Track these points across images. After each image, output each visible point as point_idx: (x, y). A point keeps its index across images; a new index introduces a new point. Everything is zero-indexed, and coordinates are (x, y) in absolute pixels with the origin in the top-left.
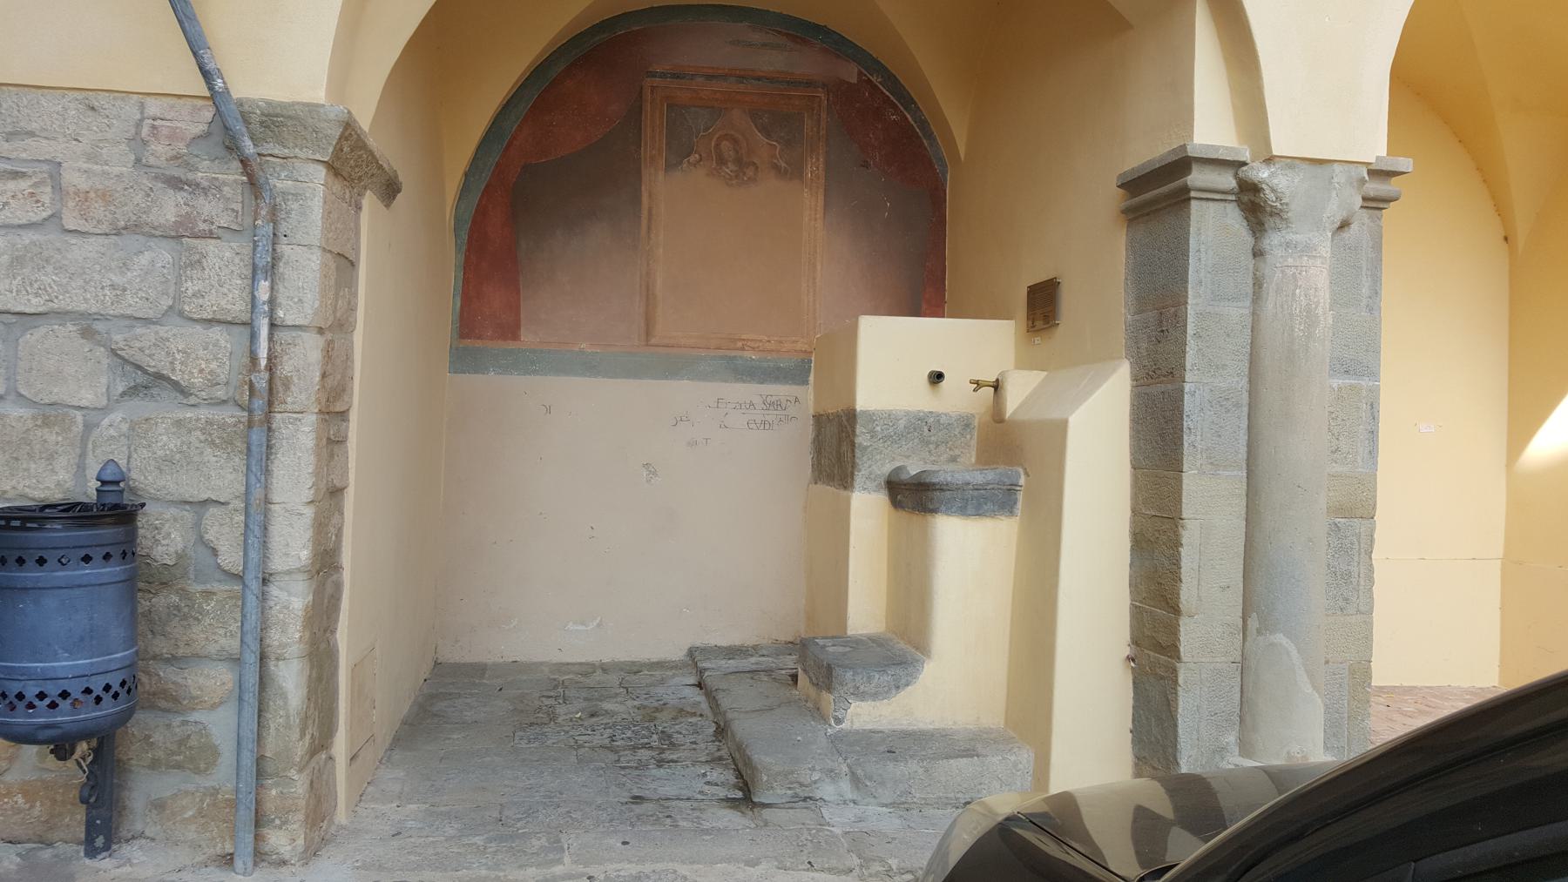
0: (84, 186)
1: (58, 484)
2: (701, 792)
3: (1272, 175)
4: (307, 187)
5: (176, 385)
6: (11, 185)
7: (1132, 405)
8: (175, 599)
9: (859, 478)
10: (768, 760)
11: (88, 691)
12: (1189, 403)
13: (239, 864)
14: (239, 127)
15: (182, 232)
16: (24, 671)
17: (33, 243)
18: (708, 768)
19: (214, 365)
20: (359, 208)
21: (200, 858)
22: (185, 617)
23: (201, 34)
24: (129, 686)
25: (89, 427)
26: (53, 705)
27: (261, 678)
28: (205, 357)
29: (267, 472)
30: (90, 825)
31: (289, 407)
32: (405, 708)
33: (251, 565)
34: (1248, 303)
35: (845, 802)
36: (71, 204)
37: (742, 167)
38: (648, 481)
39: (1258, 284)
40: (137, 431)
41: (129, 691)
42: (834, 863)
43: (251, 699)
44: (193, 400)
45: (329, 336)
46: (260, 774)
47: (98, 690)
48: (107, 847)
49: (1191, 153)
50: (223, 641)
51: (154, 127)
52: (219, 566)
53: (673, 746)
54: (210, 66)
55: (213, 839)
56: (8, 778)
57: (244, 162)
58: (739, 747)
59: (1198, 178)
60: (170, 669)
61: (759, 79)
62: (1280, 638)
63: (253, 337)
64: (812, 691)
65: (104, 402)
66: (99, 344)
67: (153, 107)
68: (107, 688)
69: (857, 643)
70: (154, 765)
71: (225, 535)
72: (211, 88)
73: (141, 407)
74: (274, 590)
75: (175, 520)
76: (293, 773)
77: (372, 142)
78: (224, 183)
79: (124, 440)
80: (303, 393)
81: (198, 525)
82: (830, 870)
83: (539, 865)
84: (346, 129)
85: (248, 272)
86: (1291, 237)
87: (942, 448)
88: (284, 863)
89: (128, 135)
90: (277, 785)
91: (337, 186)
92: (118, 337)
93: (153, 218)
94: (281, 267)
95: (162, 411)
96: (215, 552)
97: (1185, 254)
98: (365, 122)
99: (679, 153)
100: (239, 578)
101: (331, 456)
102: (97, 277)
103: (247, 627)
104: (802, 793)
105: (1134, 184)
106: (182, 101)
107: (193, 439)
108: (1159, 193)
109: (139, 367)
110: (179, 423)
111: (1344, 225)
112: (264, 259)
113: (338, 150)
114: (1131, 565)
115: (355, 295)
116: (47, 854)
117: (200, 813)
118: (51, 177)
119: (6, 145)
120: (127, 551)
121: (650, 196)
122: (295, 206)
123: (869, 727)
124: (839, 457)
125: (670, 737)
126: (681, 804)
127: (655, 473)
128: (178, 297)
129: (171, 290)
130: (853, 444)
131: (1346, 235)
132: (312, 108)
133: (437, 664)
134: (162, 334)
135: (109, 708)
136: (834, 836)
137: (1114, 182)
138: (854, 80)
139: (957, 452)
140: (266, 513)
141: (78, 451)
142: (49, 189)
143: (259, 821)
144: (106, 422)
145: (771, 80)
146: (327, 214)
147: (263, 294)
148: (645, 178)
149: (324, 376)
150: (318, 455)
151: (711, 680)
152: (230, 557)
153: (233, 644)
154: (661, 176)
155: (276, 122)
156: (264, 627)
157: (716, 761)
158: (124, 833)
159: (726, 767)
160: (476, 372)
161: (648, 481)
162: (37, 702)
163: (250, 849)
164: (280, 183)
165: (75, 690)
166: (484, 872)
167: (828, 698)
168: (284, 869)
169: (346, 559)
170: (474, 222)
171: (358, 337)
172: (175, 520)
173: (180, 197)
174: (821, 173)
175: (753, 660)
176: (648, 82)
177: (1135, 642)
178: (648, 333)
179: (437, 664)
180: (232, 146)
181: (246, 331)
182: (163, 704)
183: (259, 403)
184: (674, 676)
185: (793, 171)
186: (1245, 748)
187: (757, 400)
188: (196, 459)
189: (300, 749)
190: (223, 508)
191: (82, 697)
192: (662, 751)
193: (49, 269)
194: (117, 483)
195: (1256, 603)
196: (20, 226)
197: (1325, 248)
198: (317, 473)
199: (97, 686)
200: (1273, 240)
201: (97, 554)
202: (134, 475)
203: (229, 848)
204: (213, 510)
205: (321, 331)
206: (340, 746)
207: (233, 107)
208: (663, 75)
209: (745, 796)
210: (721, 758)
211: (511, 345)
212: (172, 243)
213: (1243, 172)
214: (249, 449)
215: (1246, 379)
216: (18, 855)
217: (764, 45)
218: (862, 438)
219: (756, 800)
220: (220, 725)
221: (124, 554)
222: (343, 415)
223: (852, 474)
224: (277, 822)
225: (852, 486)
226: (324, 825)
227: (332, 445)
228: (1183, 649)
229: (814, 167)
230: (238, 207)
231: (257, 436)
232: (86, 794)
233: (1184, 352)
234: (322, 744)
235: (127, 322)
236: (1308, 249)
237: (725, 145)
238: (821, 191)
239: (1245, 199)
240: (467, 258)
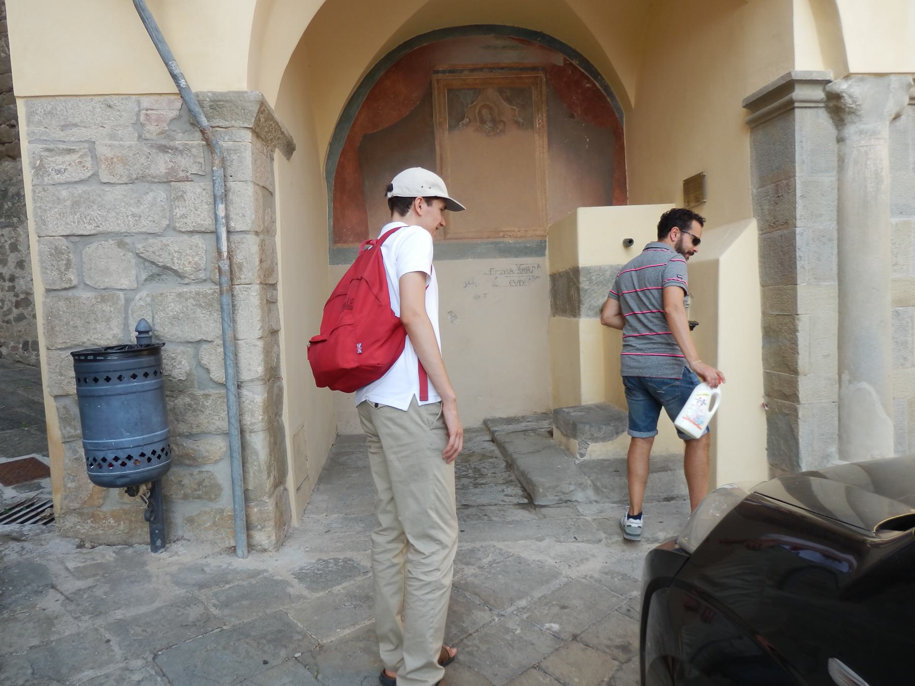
0: (110, 155)
1: (114, 336)
2: (502, 501)
3: (850, 86)
4: (241, 145)
5: (175, 272)
6: (68, 158)
7: (760, 247)
8: (188, 400)
9: (584, 309)
10: (542, 480)
11: (143, 455)
12: (799, 241)
13: (239, 552)
14: (197, 109)
15: (170, 179)
16: (104, 445)
17: (84, 192)
18: (504, 487)
19: (197, 259)
20: (272, 159)
21: (217, 550)
22: (195, 411)
23: (169, 52)
24: (166, 451)
25: (128, 301)
26: (124, 464)
27: (242, 443)
28: (190, 254)
29: (234, 321)
30: (152, 534)
31: (243, 281)
33: (230, 377)
34: (835, 173)
35: (591, 502)
36: (103, 166)
37: (496, 124)
38: (452, 322)
39: (841, 160)
40: (156, 302)
41: (167, 454)
43: (237, 456)
44: (186, 281)
45: (262, 236)
46: (247, 499)
47: (148, 454)
48: (163, 546)
49: (795, 77)
50: (218, 423)
51: (147, 115)
52: (211, 379)
53: (482, 475)
54: (176, 72)
55: (223, 538)
56: (104, 509)
57: (203, 132)
58: (523, 474)
59: (799, 93)
60: (189, 441)
61: (502, 68)
62: (864, 385)
63: (218, 239)
64: (564, 439)
65: (135, 286)
66: (129, 250)
67: (146, 102)
68: (154, 452)
69: (588, 409)
70: (186, 497)
71: (213, 359)
72: (178, 86)
73: (155, 287)
74: (245, 392)
75: (184, 353)
76: (265, 498)
77: (277, 116)
78: (192, 147)
79: (149, 308)
80: (249, 273)
81: (196, 355)
82: (588, 541)
84: (261, 106)
85: (211, 200)
86: (862, 127)
88: (265, 550)
89: (133, 121)
90: (257, 505)
91: (259, 144)
92: (140, 246)
93: (153, 171)
94: (231, 196)
95: (170, 289)
96: (208, 371)
97: (792, 144)
98: (272, 102)
99: (457, 118)
100: (224, 385)
101: (270, 311)
102: (123, 210)
103: (231, 414)
104: (564, 498)
105: (753, 104)
106: (162, 97)
107: (189, 304)
108: (773, 108)
109: (153, 263)
110: (180, 295)
111: (897, 117)
112: (220, 191)
113: (258, 120)
114: (764, 347)
115: (275, 212)
116: (130, 551)
117: (214, 524)
118: (90, 150)
119: (62, 133)
120: (157, 371)
121: (441, 146)
122: (235, 157)
123: (601, 457)
124: (570, 299)
125: (479, 470)
126: (493, 508)
127: (456, 317)
128: (172, 219)
129: (168, 215)
130: (578, 289)
131: (898, 123)
132: (240, 94)
133: (338, 436)
134: (164, 241)
135: (156, 465)
136: (586, 521)
137: (740, 104)
138: (561, 63)
140: (236, 346)
141: (123, 315)
142: (90, 158)
143: (249, 527)
144: (137, 297)
145: (510, 68)
146: (255, 161)
147: (221, 212)
149: (261, 261)
150: (262, 309)
151: (499, 436)
152: (218, 374)
153: (224, 425)
154: (446, 133)
155: (219, 104)
156: (241, 414)
157: (508, 482)
158: (172, 537)
159: (515, 486)
161: (452, 322)
162: (114, 463)
163: (245, 543)
164: (225, 143)
165: (135, 454)
167: (574, 443)
168: (266, 554)
169: (283, 372)
170: (337, 172)
171: (278, 239)
172: (184, 353)
173: (167, 157)
175: (523, 424)
176: (435, 77)
177: (768, 394)
180: (194, 123)
181: (213, 237)
182: (187, 462)
183: (225, 279)
184: (477, 436)
185: (527, 124)
186: (842, 454)
187: (515, 268)
188: (192, 316)
189: (268, 485)
190: (210, 345)
191: (140, 459)
192: (476, 479)
193: (95, 207)
194: (147, 332)
195: (847, 365)
196: (76, 182)
197: (885, 129)
198: (263, 320)
199: (148, 452)
200: (851, 130)
201: (140, 374)
202: (157, 327)
203: (233, 543)
204: (205, 346)
205: (257, 233)
206: (291, 482)
207: (193, 97)
208: (444, 72)
209: (530, 501)
210: (511, 481)
212: (165, 186)
213: (829, 87)
214: (222, 308)
215: (835, 222)
216: (114, 552)
217: (504, 47)
218: (584, 284)
219: (536, 503)
220: (221, 472)
221: (155, 373)
222: (274, 286)
223: (579, 307)
224: (259, 527)
225: (580, 315)
226: (286, 528)
227: (270, 303)
228: (803, 394)
229: (540, 121)
230: (202, 160)
231: (226, 299)
232: (148, 515)
233: (795, 208)
234: (280, 481)
235: (144, 236)
236: (874, 134)
238: (546, 134)
239: (831, 104)
240: (335, 195)
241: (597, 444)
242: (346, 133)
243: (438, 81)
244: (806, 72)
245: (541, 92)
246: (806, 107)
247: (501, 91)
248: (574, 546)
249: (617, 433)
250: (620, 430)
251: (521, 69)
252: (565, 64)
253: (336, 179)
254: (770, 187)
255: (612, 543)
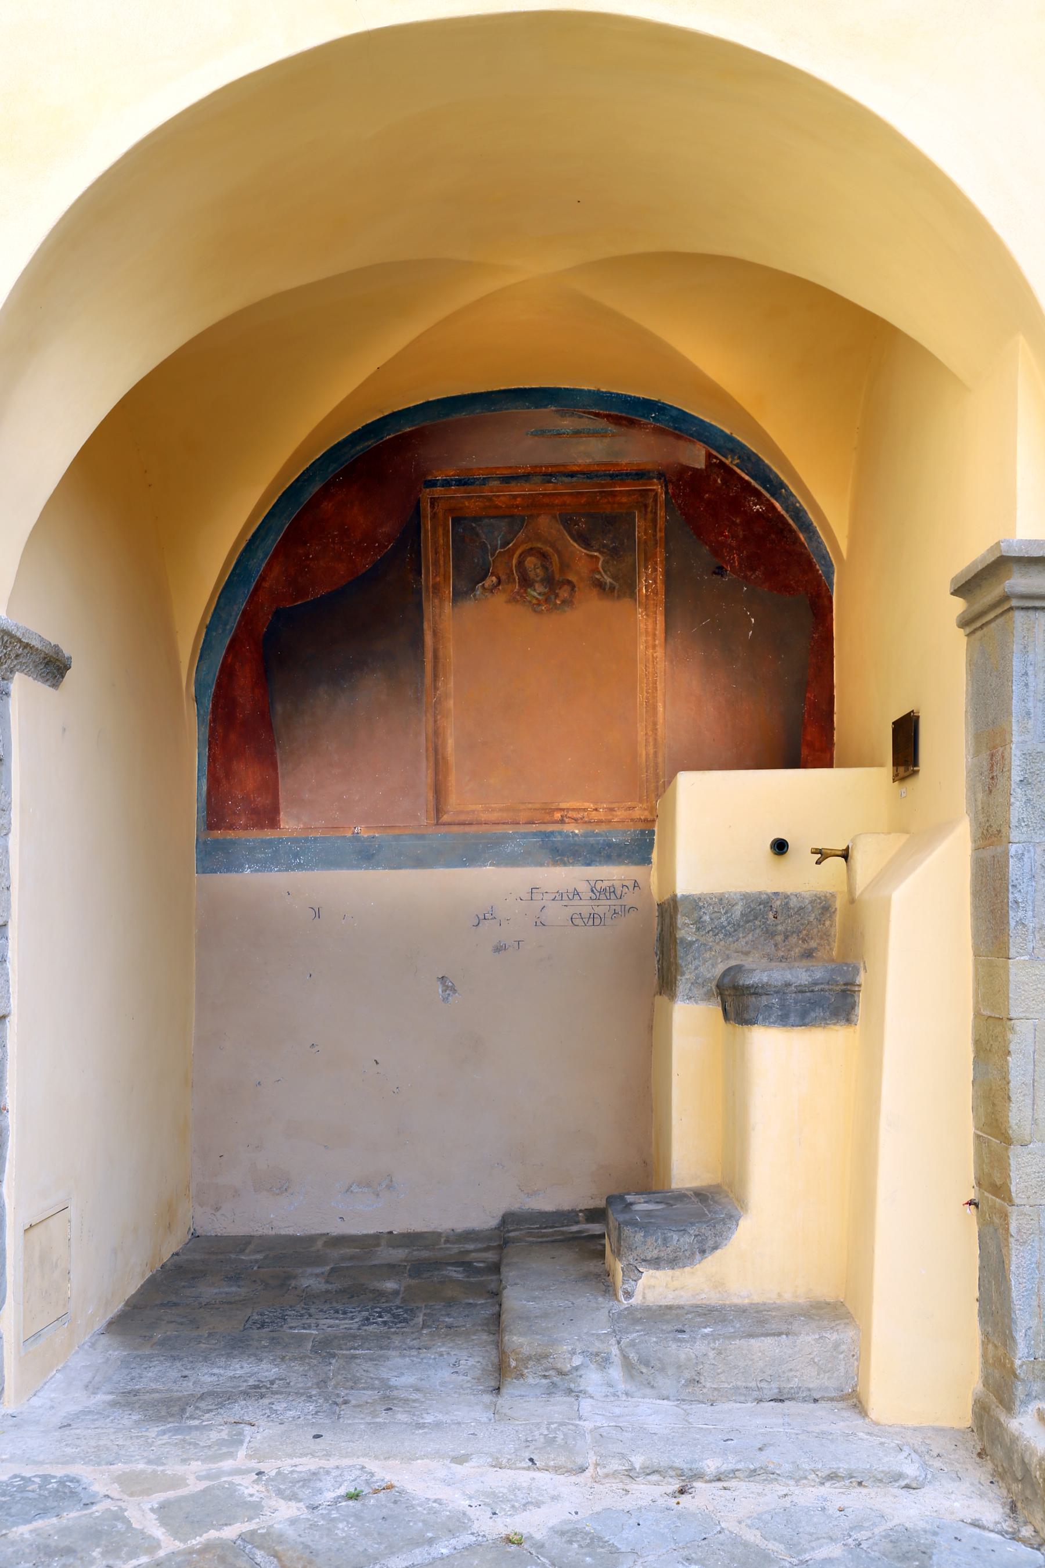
9: (682, 985)
32: (132, 1288)
37: (553, 587)
38: (445, 1000)
42: (562, 1460)
61: (572, 475)
82: (557, 1469)
83: (204, 1461)
87: (793, 939)
121: (435, 633)
138: (700, 464)
139: (813, 944)
145: (588, 474)
148: (429, 610)
154: (448, 607)
160: (229, 871)
161: (445, 1000)
166: (141, 1466)
170: (219, 686)
174: (660, 586)
176: (427, 494)
178: (439, 811)
179: (195, 1236)
185: (622, 587)
208: (447, 483)
211: (269, 834)
229: (650, 581)
237: (531, 562)
240: (212, 731)
241: (659, 1274)
242: (240, 605)
243: (433, 501)
244: (1030, 543)
245: (654, 521)
246: (1035, 608)
247: (567, 521)
248: (524, 1477)
249: (703, 1252)
250: (711, 1243)
251: (612, 476)
252: (709, 464)
253: (216, 697)
254: (985, 755)
255: (607, 1476)
